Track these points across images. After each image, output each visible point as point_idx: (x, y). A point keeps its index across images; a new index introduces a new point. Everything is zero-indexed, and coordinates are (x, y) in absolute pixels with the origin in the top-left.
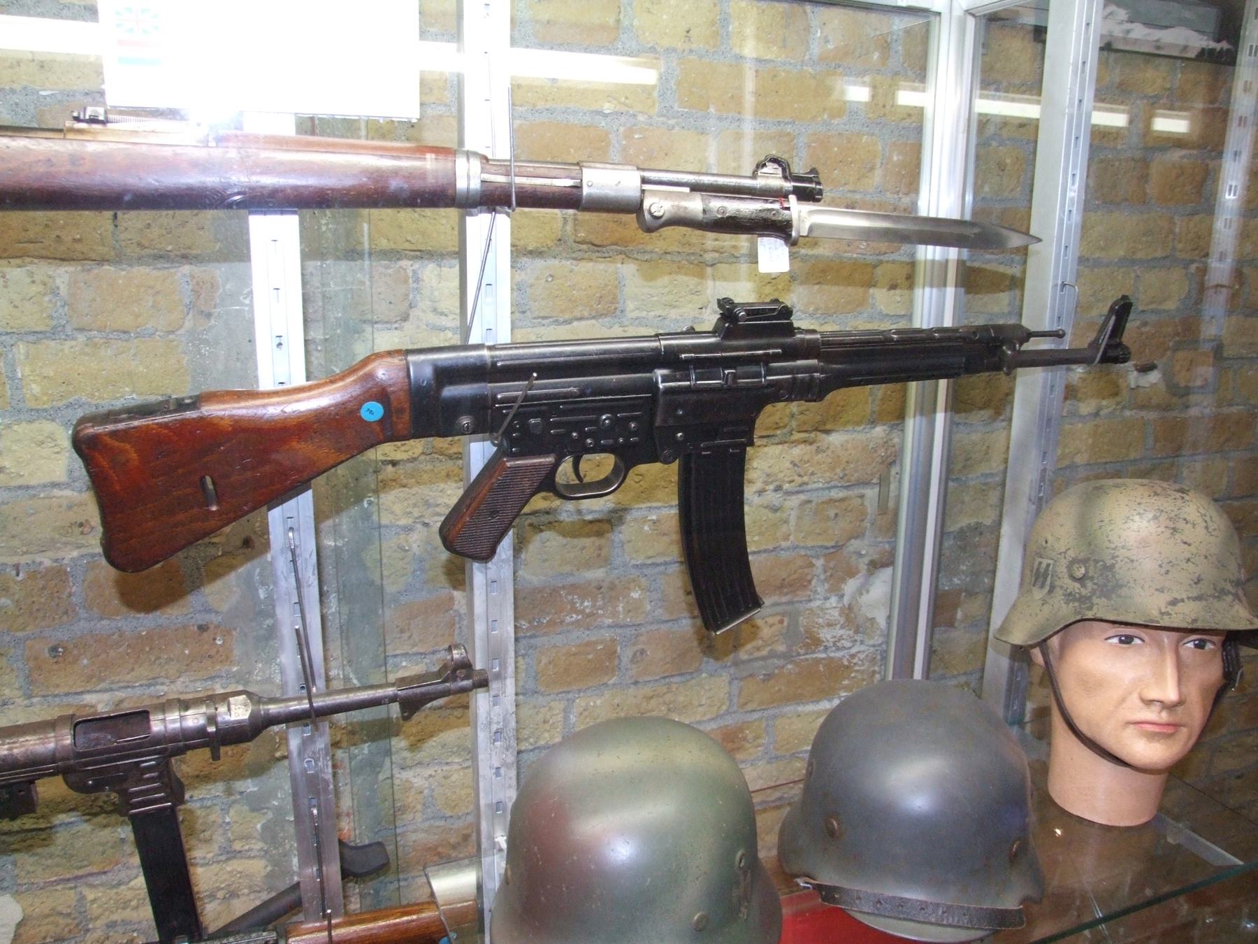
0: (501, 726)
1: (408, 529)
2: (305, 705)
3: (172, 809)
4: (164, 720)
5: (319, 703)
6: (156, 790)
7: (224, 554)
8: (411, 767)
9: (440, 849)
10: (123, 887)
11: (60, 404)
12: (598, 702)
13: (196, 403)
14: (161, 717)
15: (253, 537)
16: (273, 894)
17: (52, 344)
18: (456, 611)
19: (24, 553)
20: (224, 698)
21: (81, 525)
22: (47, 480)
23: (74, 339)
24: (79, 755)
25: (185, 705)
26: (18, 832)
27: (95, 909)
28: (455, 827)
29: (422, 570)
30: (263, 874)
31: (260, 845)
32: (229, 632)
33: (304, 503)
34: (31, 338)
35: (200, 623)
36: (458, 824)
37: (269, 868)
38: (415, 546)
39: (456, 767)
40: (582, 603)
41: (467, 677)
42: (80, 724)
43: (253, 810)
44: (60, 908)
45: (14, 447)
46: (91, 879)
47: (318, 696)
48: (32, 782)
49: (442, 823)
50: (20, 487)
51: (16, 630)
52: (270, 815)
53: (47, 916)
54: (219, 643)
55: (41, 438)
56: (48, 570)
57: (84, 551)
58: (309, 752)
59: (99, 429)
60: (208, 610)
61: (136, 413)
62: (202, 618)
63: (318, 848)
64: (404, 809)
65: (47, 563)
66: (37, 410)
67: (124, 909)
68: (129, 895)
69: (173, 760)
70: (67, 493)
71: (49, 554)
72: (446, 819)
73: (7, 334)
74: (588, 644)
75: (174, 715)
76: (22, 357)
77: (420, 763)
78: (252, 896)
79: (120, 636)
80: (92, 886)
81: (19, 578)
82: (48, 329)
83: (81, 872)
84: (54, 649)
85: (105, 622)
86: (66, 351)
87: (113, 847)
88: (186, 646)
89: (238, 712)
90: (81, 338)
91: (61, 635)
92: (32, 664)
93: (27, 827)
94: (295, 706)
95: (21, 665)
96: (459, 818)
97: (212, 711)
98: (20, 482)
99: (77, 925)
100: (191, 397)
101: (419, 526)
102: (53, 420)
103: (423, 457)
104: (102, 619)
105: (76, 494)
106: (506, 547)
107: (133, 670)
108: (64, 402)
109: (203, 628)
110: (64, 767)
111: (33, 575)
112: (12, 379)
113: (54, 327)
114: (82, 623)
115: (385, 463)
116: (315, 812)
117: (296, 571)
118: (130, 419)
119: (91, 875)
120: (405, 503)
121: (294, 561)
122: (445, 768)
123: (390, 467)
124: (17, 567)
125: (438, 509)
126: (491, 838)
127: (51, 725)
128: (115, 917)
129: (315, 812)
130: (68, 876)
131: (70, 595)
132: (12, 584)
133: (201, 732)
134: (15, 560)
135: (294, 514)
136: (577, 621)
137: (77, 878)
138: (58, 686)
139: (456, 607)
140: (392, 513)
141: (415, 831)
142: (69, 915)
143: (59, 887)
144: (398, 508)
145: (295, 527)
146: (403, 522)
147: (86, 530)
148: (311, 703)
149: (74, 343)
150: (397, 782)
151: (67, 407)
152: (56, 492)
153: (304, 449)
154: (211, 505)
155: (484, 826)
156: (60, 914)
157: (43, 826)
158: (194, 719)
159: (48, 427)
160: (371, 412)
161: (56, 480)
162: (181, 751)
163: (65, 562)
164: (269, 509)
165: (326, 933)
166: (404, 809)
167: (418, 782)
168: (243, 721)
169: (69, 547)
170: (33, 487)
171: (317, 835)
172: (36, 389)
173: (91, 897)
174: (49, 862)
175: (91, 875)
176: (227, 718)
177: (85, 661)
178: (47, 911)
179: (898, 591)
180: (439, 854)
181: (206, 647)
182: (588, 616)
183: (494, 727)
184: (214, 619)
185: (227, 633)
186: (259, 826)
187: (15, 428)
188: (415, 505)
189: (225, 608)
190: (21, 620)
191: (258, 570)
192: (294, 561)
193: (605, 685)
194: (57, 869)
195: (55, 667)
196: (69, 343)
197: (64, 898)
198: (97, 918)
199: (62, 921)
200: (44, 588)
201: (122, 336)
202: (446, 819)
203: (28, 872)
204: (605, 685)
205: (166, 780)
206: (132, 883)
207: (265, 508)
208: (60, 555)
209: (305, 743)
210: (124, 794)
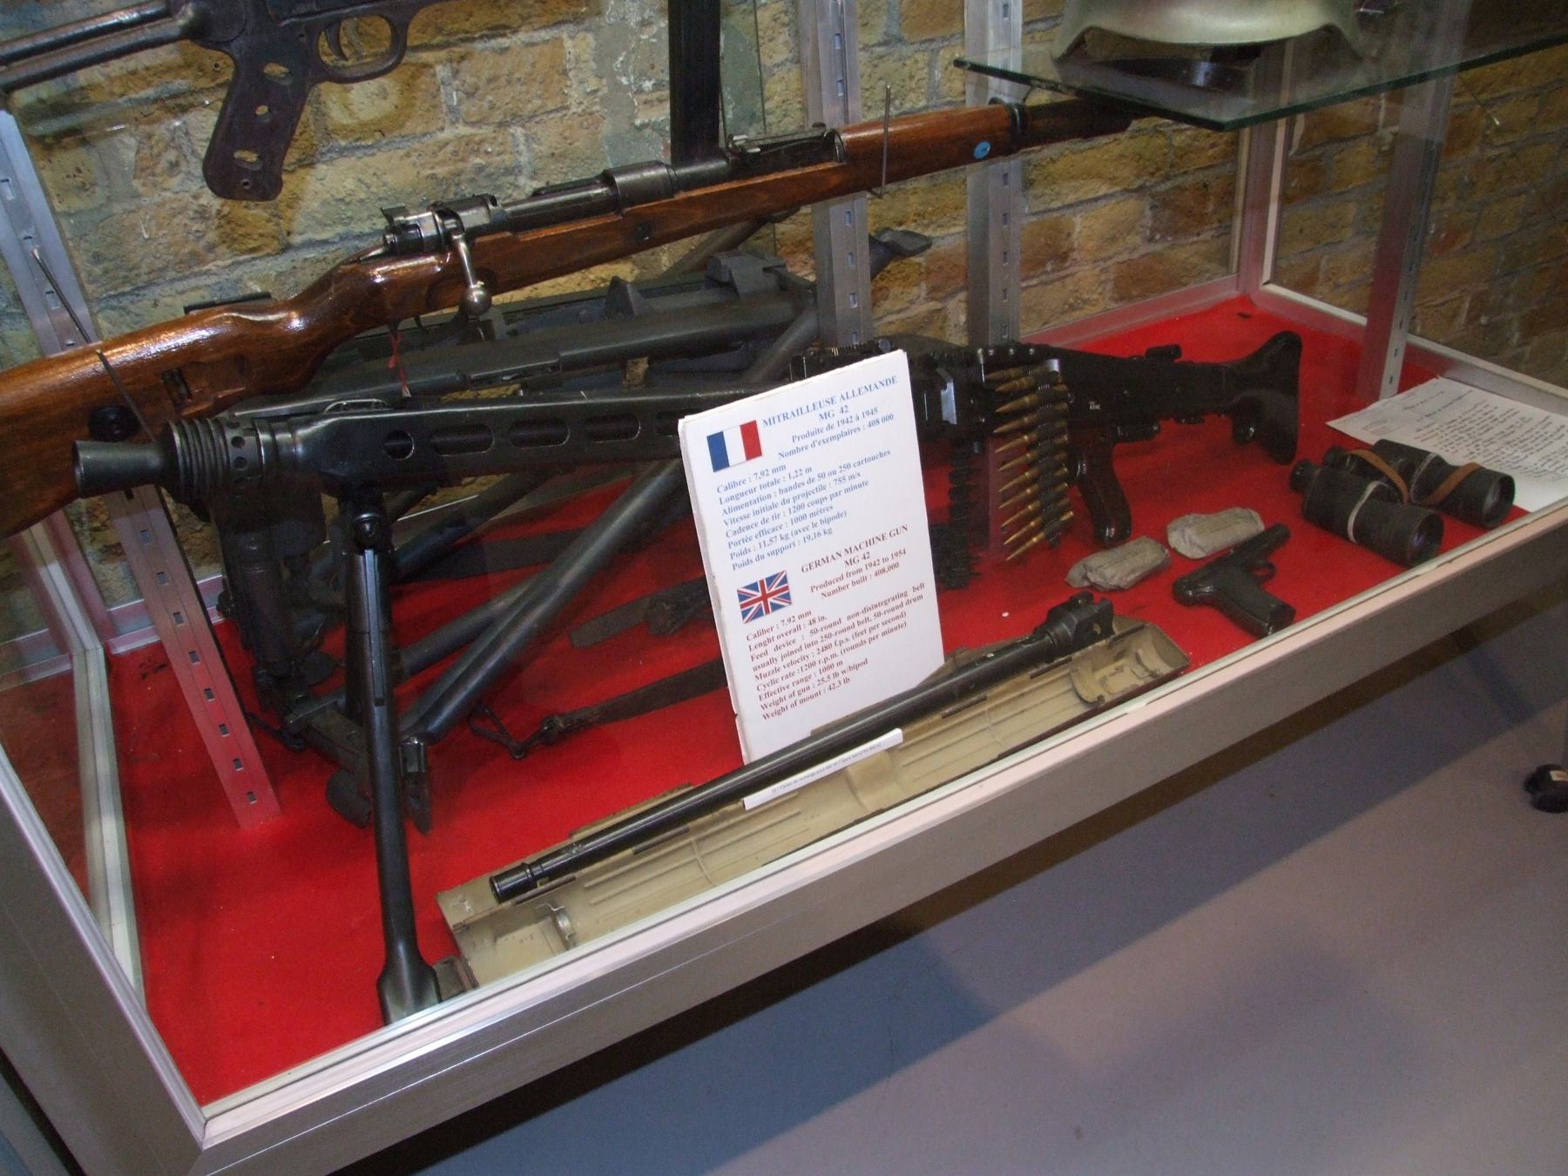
26: (369, 235)
63: (843, 52)
100: (65, 148)
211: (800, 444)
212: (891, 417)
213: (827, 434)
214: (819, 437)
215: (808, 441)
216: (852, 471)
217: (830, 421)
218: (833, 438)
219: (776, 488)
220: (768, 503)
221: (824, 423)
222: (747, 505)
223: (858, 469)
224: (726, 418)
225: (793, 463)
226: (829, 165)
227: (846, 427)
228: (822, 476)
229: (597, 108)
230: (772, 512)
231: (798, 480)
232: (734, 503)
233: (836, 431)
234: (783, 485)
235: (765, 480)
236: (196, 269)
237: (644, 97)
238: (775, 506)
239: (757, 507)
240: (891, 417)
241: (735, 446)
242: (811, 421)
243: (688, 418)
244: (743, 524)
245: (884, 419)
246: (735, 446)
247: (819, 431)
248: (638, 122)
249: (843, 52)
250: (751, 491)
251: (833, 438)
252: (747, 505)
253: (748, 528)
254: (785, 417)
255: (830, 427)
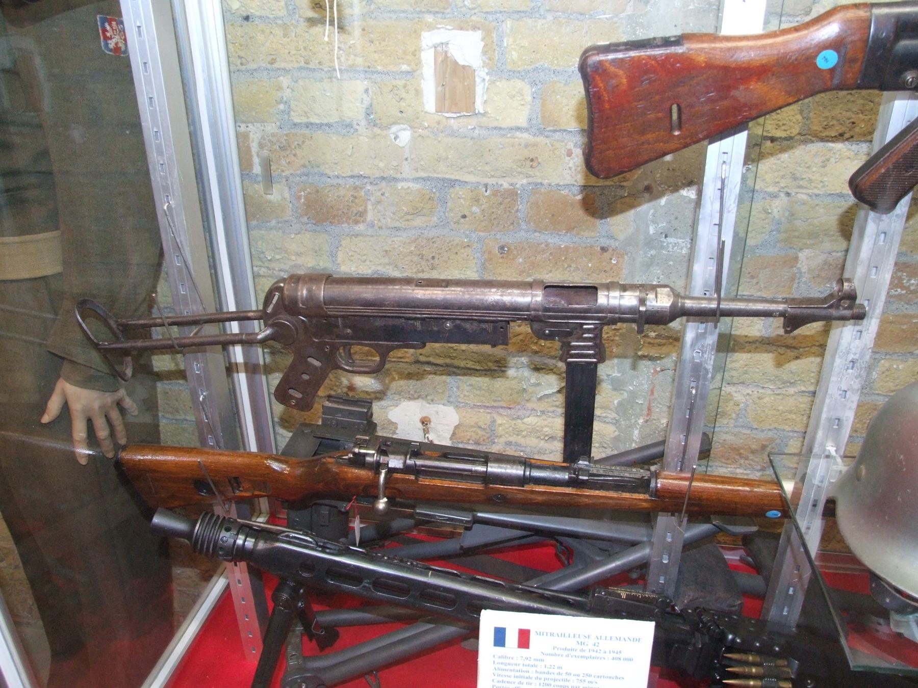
0: (857, 357)
1: (774, 196)
2: (713, 305)
3: (596, 364)
4: (608, 296)
5: (724, 305)
6: (588, 348)
7: (629, 195)
8: (734, 384)
9: (742, 451)
10: (519, 421)
11: (530, 68)
12: (901, 367)
13: (679, 41)
14: (606, 293)
15: (653, 185)
16: (616, 452)
17: (529, 21)
18: (799, 269)
19: (493, 176)
20: (654, 288)
21: (532, 160)
22: (513, 125)
23: (545, 18)
24: (546, 310)
25: (624, 288)
26: (463, 368)
27: (500, 431)
28: (757, 437)
29: (779, 231)
30: (612, 436)
31: (614, 415)
32: (622, 256)
33: (738, 142)
34: (516, 16)
35: (603, 245)
36: (762, 436)
37: (617, 433)
38: (775, 210)
39: (769, 392)
40: (910, 280)
41: (850, 307)
42: (549, 287)
43: (615, 389)
44: (480, 424)
45: (495, 98)
46: (501, 411)
47: (725, 300)
48: (508, 322)
49: (748, 432)
50: (495, 128)
51: (480, 231)
52: (625, 395)
53: (472, 427)
54: (614, 262)
55: (514, 93)
56: (506, 191)
57: (531, 180)
58: (699, 345)
59: (602, 57)
60: (612, 237)
61: (632, 46)
62: (604, 242)
63: (690, 420)
64: (724, 414)
65: (506, 185)
66: (514, 72)
67: (518, 435)
68: (522, 427)
69: (606, 328)
70: (525, 135)
71: (507, 179)
72: (752, 429)
73: (501, 12)
74: (905, 316)
75: (615, 294)
76: (508, 31)
77: (743, 383)
78: (600, 450)
79: (546, 246)
80: (501, 415)
81: (487, 194)
82: (529, 9)
83: (495, 404)
84: (502, 248)
85: (537, 234)
86: (539, 28)
87: (518, 393)
88: (590, 261)
89: (661, 301)
90: (550, 17)
91: (507, 239)
92: (486, 256)
93: (468, 366)
94: (704, 305)
95: (479, 255)
96: (763, 431)
97: (643, 295)
98: (495, 124)
99: (488, 438)
100: (675, 37)
101: (782, 195)
102: (523, 80)
103: (798, 137)
104: (535, 231)
105: (531, 137)
106: (904, 205)
107: (551, 272)
108: (533, 66)
109: (604, 249)
110: (536, 319)
111: (495, 193)
112: (500, 47)
113: (533, 8)
114: (522, 233)
115: (765, 138)
116: (694, 392)
117: (722, 198)
118: (627, 50)
119: (502, 407)
120: (776, 174)
121: (722, 190)
122: (761, 391)
123: (768, 143)
124: (486, 186)
125: (801, 183)
126: (823, 445)
127: (530, 285)
128: (511, 439)
129: (694, 392)
130: (487, 405)
131: (517, 211)
132: (481, 197)
133: (632, 310)
134: (486, 180)
135: (729, 151)
136: (900, 295)
137: (493, 407)
138: (500, 274)
139: (799, 265)
140: (764, 180)
141: (727, 433)
142: (484, 429)
143: (482, 410)
144: (769, 177)
145: (728, 162)
146: (771, 189)
147: (535, 164)
148: (719, 304)
149: (544, 21)
150: (723, 393)
151: (534, 70)
152: (518, 134)
153: (757, 89)
154: (675, 130)
155: (820, 434)
156: (480, 427)
157: (478, 368)
158: (629, 300)
159: (519, 84)
160: (826, 60)
161: (519, 125)
162: (613, 321)
163: (518, 186)
164: (710, 143)
165: (687, 483)
166: (724, 414)
167: (738, 397)
168: (666, 307)
169: (521, 176)
170: (504, 129)
171: (691, 410)
172: (515, 55)
173: (499, 422)
174: (478, 392)
175: (502, 407)
176: (654, 303)
177: (521, 260)
178: (472, 424)
179: (446, 483)
180: (740, 454)
181: (604, 264)
182: (912, 292)
183: (851, 357)
184: (612, 244)
185: (620, 256)
186: (616, 402)
187: (498, 83)
188: (783, 177)
189: (622, 237)
190: (483, 224)
191: (652, 211)
192: (722, 190)
193: (912, 353)
194: (483, 399)
195: (501, 260)
196: (540, 22)
197: (484, 417)
198: (501, 436)
199: (480, 432)
200: (501, 204)
201: (579, 17)
202: (752, 429)
203: (465, 396)
204: (912, 353)
205: (598, 342)
206: (526, 420)
207: (706, 142)
208: (514, 180)
209: (699, 337)
210: (567, 347)
211: (558, 652)
212: (631, 660)
213: (578, 653)
214: (573, 653)
215: (566, 653)
216: (592, 679)
217: (584, 647)
218: (582, 657)
219: (534, 669)
220: (527, 675)
221: (579, 647)
222: (511, 670)
223: (596, 679)
224: (513, 621)
225: (549, 661)
226: (641, 496)
227: (594, 654)
228: (568, 674)
229: (617, 338)
230: (528, 680)
231: (551, 671)
232: (503, 667)
233: (586, 654)
234: (539, 669)
235: (527, 662)
236: (370, 358)
237: (649, 340)
238: (530, 678)
239: (518, 674)
240: (631, 660)
241: (512, 638)
242: (571, 643)
243: (488, 611)
244: (506, 679)
245: (625, 659)
246: (512, 638)
247: (573, 650)
248: (640, 353)
249: (690, 420)
250: (516, 665)
251: (582, 657)
252: (511, 670)
253: (508, 682)
254: (552, 635)
255: (582, 650)
